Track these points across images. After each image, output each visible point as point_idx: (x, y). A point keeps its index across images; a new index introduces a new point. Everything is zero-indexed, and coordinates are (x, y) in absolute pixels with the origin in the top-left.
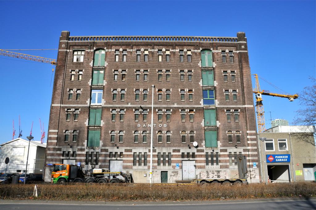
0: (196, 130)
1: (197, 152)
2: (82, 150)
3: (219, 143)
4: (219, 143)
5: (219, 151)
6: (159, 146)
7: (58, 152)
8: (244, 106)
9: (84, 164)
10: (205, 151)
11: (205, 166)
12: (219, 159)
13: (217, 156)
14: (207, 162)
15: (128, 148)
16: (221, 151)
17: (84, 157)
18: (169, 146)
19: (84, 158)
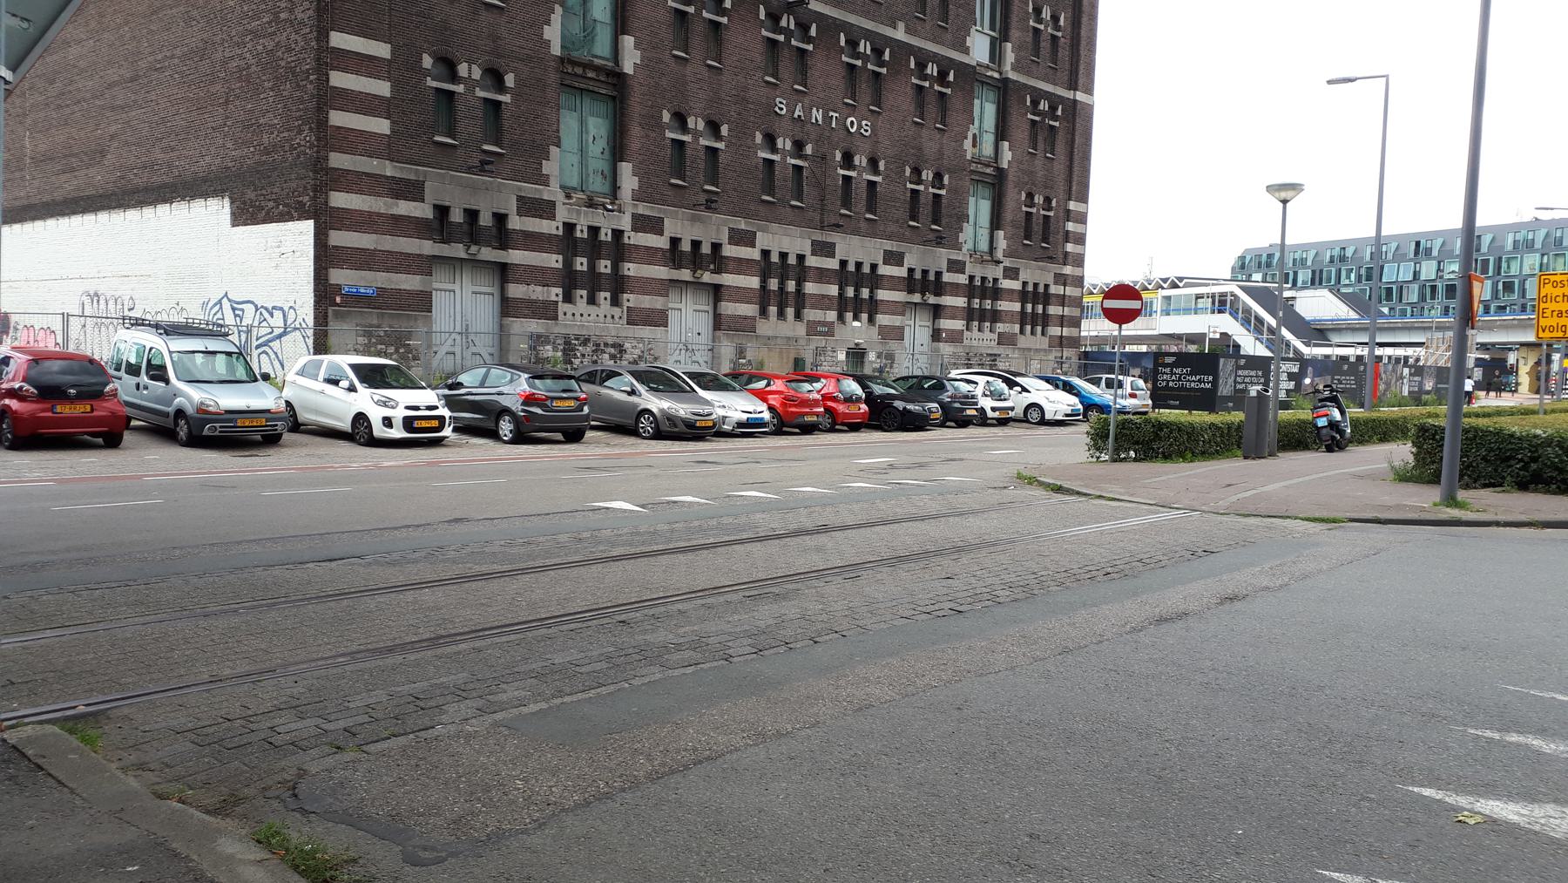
0: (950, 172)
1: (635, 229)
2: (544, 209)
3: (629, 181)
4: (629, 181)
5: (625, 223)
6: (679, 197)
7: (405, 208)
8: (1069, 94)
9: (554, 298)
10: (562, 214)
11: (754, 318)
12: (631, 269)
13: (619, 249)
14: (569, 282)
15: (742, 225)
16: (641, 223)
17: (555, 257)
18: (872, 231)
19: (810, 288)
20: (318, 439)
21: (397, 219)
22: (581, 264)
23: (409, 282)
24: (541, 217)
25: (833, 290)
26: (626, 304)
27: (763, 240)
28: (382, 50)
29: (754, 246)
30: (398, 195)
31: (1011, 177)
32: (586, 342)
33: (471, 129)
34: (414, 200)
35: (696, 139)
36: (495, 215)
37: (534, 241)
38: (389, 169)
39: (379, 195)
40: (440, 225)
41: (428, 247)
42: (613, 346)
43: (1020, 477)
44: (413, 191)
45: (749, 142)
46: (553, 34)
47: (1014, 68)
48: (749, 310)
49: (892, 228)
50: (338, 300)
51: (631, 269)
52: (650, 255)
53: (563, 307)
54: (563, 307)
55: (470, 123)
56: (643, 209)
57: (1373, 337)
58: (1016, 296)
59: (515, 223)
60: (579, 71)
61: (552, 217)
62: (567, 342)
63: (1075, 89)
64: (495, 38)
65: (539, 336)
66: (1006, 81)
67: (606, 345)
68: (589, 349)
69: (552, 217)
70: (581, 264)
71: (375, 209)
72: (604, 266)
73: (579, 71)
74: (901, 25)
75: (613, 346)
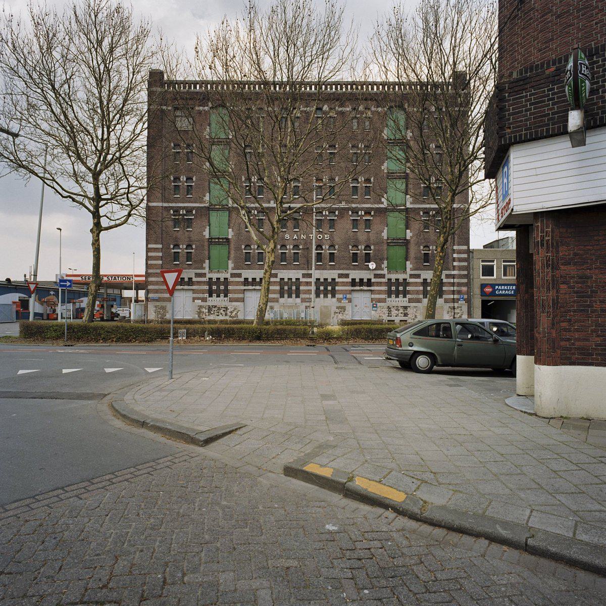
1: (410, 278)
14: (389, 293)
22: (401, 288)
23: (241, 296)
25: (206, 287)
28: (160, 246)
31: (412, 242)
35: (183, 250)
36: (189, 278)
37: (379, 284)
41: (243, 288)
43: (360, 363)
46: (206, 234)
47: (411, 203)
48: (383, 296)
49: (345, 266)
51: (206, 287)
53: (387, 299)
54: (208, 299)
55: (183, 258)
56: (413, 272)
57: (494, 290)
59: (194, 279)
60: (217, 240)
61: (205, 277)
65: (201, 306)
69: (205, 277)
70: (222, 287)
72: (214, 287)
73: (217, 240)
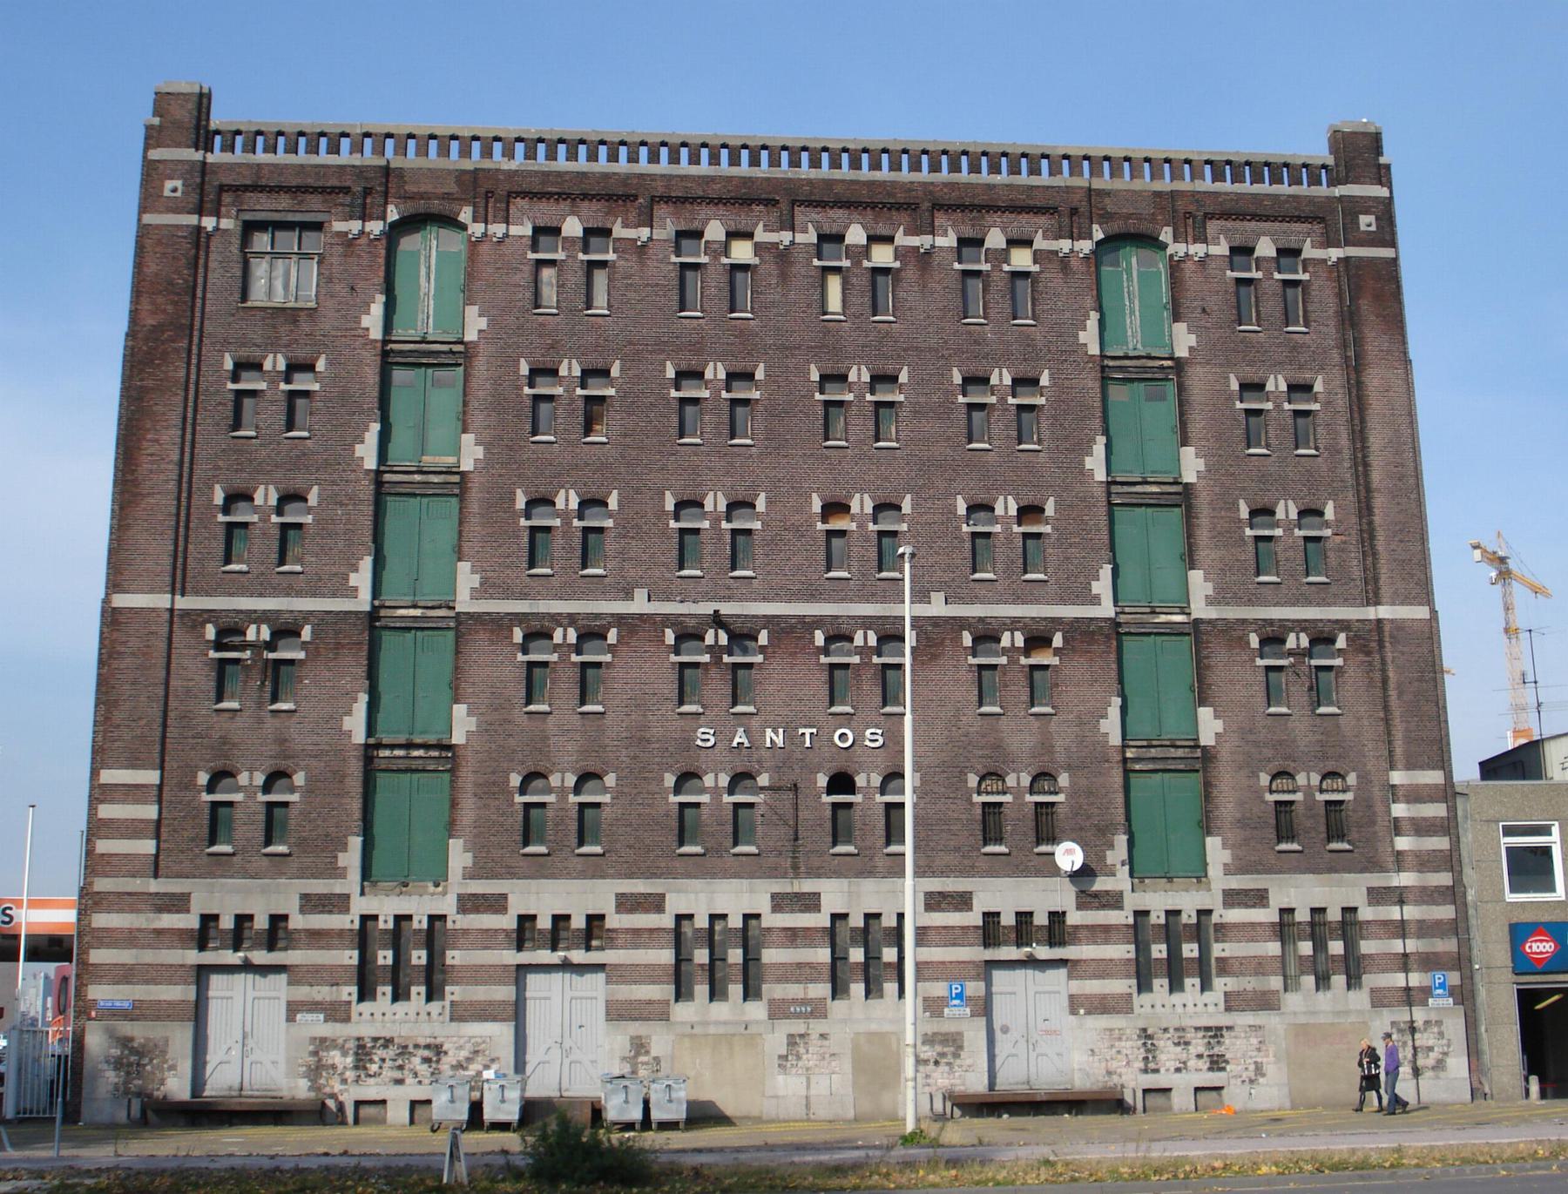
1: (302, 911)
9: (345, 997)
11: (667, 1002)
15: (639, 886)
17: (348, 953)
20: (808, 1138)
21: (159, 932)
24: (330, 912)
26: (449, 998)
27: (1278, 899)
29: (1121, 908)
30: (160, 909)
31: (1224, 754)
32: (388, 1042)
33: (250, 835)
34: (178, 912)
38: (154, 886)
39: (138, 911)
40: (990, 930)
42: (428, 1047)
44: (178, 903)
45: (653, 787)
47: (1210, 601)
50: (93, 1014)
52: (488, 938)
54: (356, 1008)
58: (972, 936)
62: (361, 1047)
63: (1377, 603)
64: (282, 741)
65: (323, 1040)
66: (1197, 622)
67: (417, 1046)
68: (391, 1052)
71: (136, 925)
74: (641, 594)
75: (428, 1047)
